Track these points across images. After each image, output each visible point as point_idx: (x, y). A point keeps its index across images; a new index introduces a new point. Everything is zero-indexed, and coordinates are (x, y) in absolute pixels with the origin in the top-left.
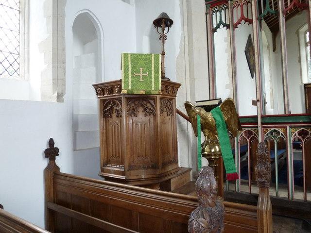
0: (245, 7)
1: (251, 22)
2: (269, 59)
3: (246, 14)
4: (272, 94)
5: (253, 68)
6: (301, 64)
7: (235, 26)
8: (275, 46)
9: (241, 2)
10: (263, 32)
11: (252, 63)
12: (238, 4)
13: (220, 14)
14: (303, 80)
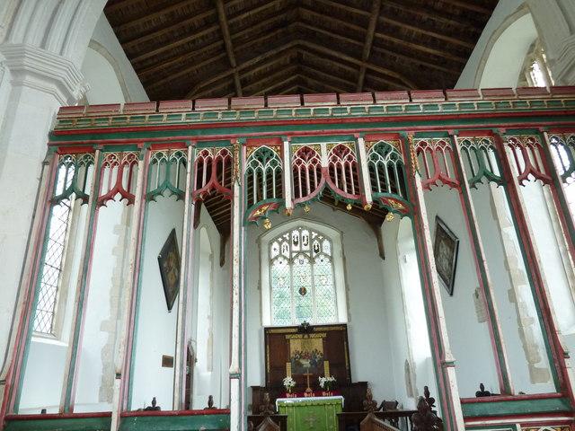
0: (126, 170)
1: (181, 196)
2: (212, 277)
3: (82, 185)
4: (211, 343)
5: (173, 292)
6: (261, 293)
7: (100, 202)
8: (143, 241)
9: (121, 158)
10: (203, 231)
11: (171, 281)
12: (115, 160)
13: (76, 172)
14: (263, 319)
